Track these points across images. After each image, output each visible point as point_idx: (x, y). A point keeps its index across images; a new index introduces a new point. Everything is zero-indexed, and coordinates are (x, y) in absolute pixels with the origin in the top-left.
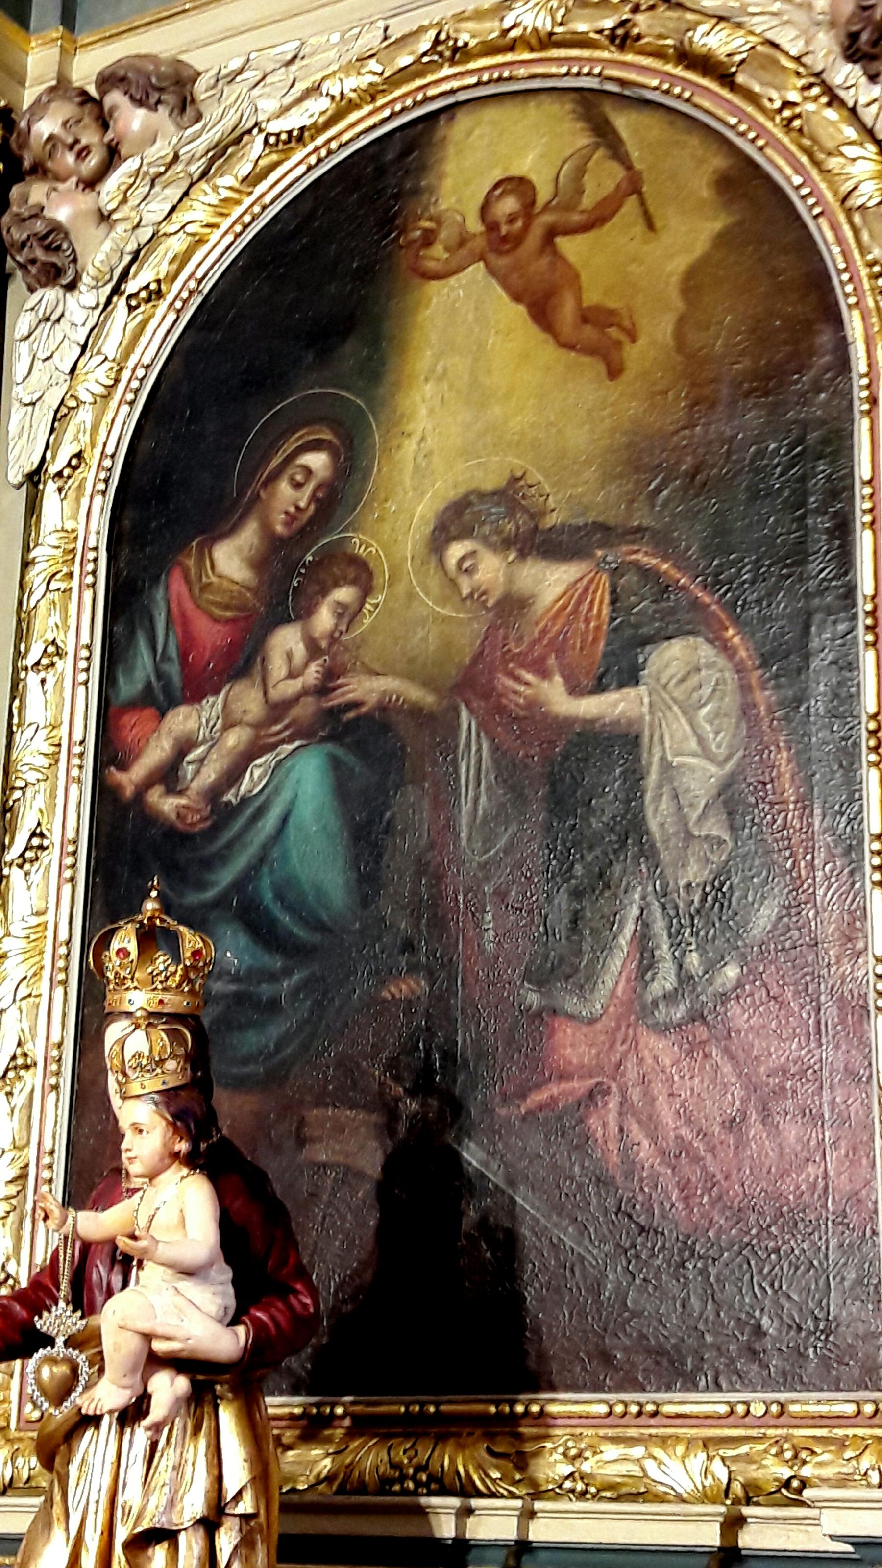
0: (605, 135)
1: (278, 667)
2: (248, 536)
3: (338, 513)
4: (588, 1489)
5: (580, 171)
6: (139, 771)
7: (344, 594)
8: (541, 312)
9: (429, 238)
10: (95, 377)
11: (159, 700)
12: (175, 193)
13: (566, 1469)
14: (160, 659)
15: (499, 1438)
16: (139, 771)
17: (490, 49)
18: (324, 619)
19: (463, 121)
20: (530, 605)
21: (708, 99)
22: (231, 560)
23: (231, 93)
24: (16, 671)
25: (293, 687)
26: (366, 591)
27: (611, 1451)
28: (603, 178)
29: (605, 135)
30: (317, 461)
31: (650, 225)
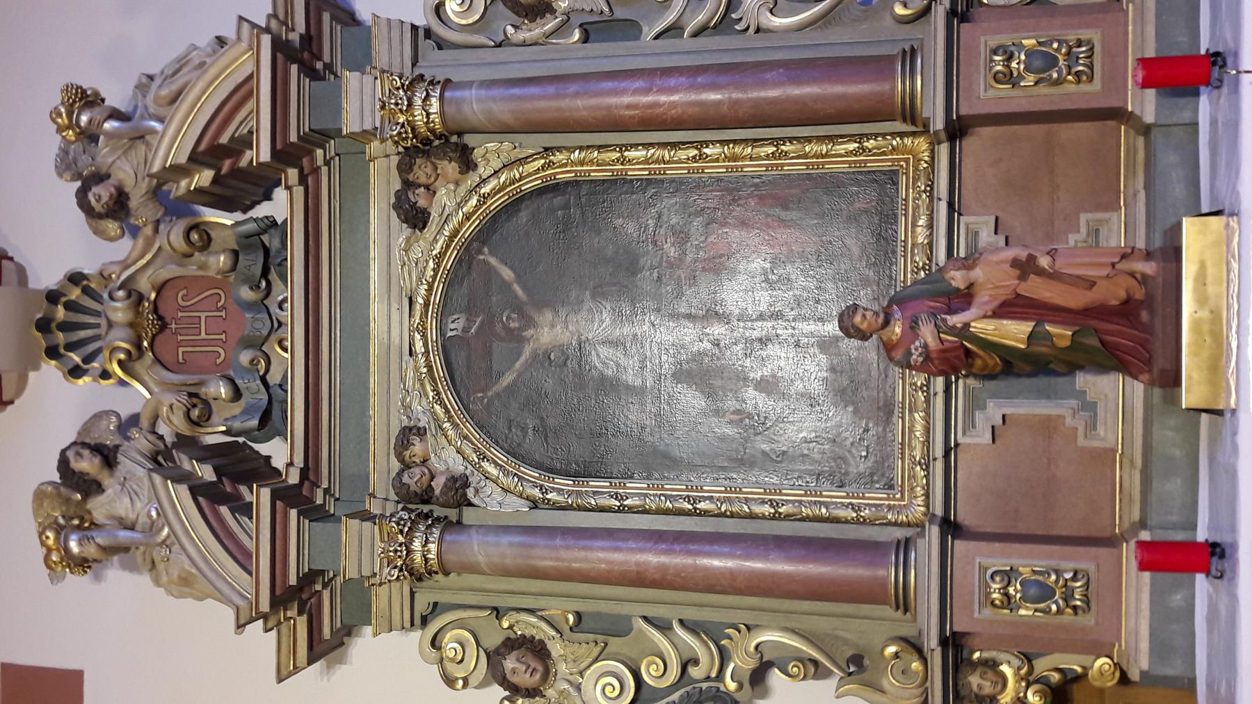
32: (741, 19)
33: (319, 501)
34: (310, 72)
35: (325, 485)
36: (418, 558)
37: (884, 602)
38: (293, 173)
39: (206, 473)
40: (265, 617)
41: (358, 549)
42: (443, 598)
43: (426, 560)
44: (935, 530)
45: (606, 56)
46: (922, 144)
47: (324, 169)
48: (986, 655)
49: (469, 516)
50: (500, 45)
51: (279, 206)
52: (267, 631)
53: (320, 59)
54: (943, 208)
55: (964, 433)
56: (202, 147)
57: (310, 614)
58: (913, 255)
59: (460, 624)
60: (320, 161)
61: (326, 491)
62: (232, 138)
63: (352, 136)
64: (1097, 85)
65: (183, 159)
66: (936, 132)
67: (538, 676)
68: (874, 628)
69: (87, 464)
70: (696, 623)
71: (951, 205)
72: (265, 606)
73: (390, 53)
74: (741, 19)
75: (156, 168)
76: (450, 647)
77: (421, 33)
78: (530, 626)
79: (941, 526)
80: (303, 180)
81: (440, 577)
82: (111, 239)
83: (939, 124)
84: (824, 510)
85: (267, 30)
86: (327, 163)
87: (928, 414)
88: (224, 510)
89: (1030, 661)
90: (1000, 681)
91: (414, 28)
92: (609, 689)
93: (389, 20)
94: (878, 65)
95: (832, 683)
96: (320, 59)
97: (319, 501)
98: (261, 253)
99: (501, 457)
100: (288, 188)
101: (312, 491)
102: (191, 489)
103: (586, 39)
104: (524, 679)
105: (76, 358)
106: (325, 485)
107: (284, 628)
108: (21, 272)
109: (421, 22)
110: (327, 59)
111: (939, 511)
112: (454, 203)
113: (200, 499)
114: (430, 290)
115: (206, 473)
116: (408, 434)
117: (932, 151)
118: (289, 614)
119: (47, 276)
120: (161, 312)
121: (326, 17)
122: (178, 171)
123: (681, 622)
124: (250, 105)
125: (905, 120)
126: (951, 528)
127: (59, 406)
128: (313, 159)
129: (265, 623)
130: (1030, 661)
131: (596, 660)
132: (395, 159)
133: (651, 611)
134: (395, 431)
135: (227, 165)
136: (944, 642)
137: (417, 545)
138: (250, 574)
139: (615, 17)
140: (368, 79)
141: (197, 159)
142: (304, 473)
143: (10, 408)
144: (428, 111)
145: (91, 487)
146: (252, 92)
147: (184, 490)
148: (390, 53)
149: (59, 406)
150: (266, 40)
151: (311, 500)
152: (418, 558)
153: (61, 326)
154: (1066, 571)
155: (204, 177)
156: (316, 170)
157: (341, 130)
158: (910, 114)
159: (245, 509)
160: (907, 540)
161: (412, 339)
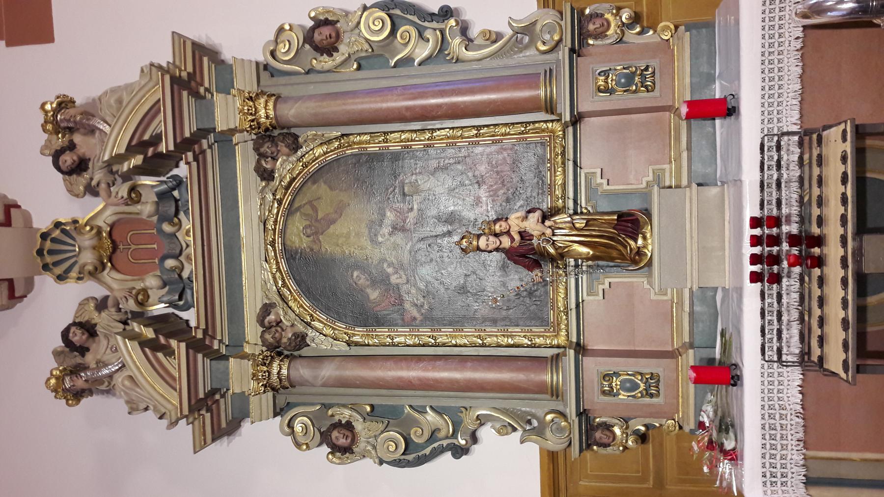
0: (298, 209)
1: (398, 281)
2: (369, 291)
3: (389, 97)
4: (564, 197)
5: (305, 215)
6: (417, 315)
7: (385, 265)
8: (333, 222)
9: (312, 250)
10: (329, 331)
11: (402, 312)
12: (290, 311)
13: (560, 201)
14: (394, 312)
15: (469, 364)
16: (417, 315)
17: (274, 235)
18: (390, 270)
19: (288, 243)
20: (350, 456)
21: (297, 184)
22: (374, 295)
23: (270, 296)
24: (394, 346)
25: (404, 277)
26: (385, 260)
27: (557, 192)
28: (308, 210)
29: (298, 209)
30: (355, 274)
31: (319, 198)
32: (449, 54)
33: (216, 347)
34: (195, 94)
35: (219, 338)
36: (274, 377)
37: (547, 393)
38: (190, 155)
39: (149, 333)
40: (186, 417)
41: (240, 376)
42: (291, 399)
43: (281, 380)
44: (572, 352)
45: (371, 79)
46: (557, 127)
47: (209, 151)
48: (604, 419)
49: (305, 352)
50: (308, 73)
51: (182, 170)
52: (188, 424)
53: (202, 85)
54: (571, 164)
55: (588, 295)
56: (134, 143)
57: (213, 415)
58: (555, 147)
59: (303, 414)
60: (205, 146)
61: (221, 341)
62: (151, 136)
63: (222, 132)
64: (656, 93)
65: (122, 150)
66: (565, 122)
67: (349, 440)
68: (541, 408)
69: (78, 337)
70: (443, 408)
71: (575, 163)
72: (186, 411)
73: (245, 82)
74: (449, 54)
75: (106, 158)
76: (298, 428)
77: (261, 67)
78: (345, 414)
79: (575, 350)
80: (196, 159)
81: (290, 389)
82: (77, 196)
83: (567, 117)
84: (510, 340)
85: (168, 72)
86: (210, 147)
87: (567, 331)
88: (160, 355)
89: (627, 422)
90: (612, 436)
91: (257, 64)
92: (392, 448)
93: (243, 60)
94: (529, 80)
95: (518, 435)
96: (202, 85)
97: (216, 347)
98: (170, 202)
99: (323, 317)
100: (187, 163)
101: (212, 343)
102: (140, 344)
103: (359, 68)
104: (342, 442)
105: (49, 259)
106: (219, 338)
107: (196, 423)
108: (27, 218)
109: (261, 58)
110: (207, 85)
111: (574, 340)
112: (285, 167)
113: (147, 350)
114: (275, 222)
115: (149, 333)
116: (267, 309)
117: (564, 132)
118: (202, 412)
119: (42, 223)
120: (114, 238)
121: (205, 59)
122: (119, 158)
123: (431, 407)
124: (157, 106)
125: (547, 112)
126: (580, 349)
127: (58, 301)
128: (201, 146)
129: (187, 420)
130: (627, 422)
131: (382, 432)
132: (250, 145)
133: (417, 402)
134: (259, 306)
135: (150, 151)
136: (579, 414)
137: (275, 370)
138: (175, 390)
139: (376, 52)
140: (230, 97)
141: (132, 149)
142: (205, 332)
143: (25, 299)
144: (265, 111)
145: (83, 350)
146: (159, 100)
147: (136, 343)
148: (245, 82)
149: (58, 301)
150: (167, 78)
151: (210, 347)
152: (274, 377)
153: (53, 250)
154: (647, 374)
155: (137, 160)
156: (203, 152)
157: (215, 129)
158: (550, 107)
159: (169, 352)
160: (558, 355)
161: (267, 250)
